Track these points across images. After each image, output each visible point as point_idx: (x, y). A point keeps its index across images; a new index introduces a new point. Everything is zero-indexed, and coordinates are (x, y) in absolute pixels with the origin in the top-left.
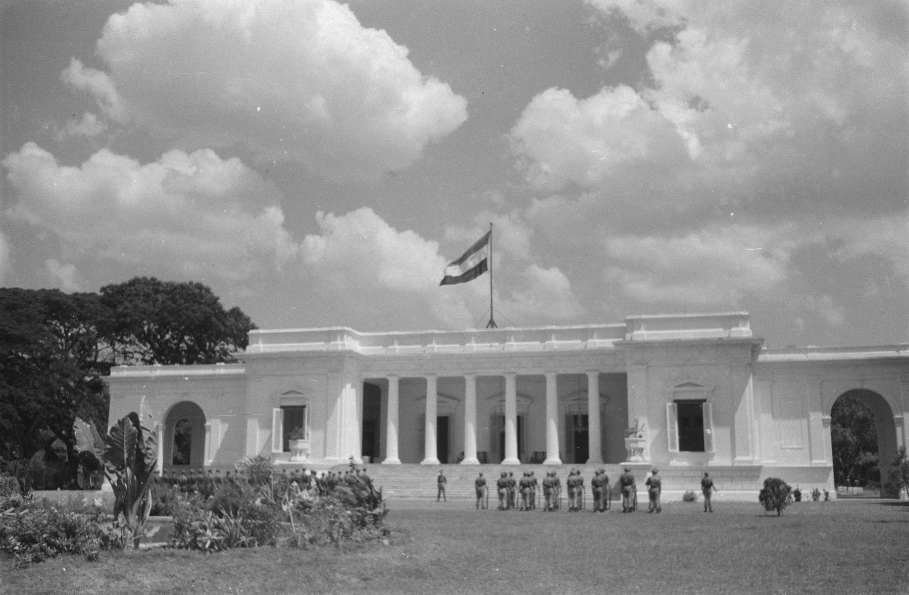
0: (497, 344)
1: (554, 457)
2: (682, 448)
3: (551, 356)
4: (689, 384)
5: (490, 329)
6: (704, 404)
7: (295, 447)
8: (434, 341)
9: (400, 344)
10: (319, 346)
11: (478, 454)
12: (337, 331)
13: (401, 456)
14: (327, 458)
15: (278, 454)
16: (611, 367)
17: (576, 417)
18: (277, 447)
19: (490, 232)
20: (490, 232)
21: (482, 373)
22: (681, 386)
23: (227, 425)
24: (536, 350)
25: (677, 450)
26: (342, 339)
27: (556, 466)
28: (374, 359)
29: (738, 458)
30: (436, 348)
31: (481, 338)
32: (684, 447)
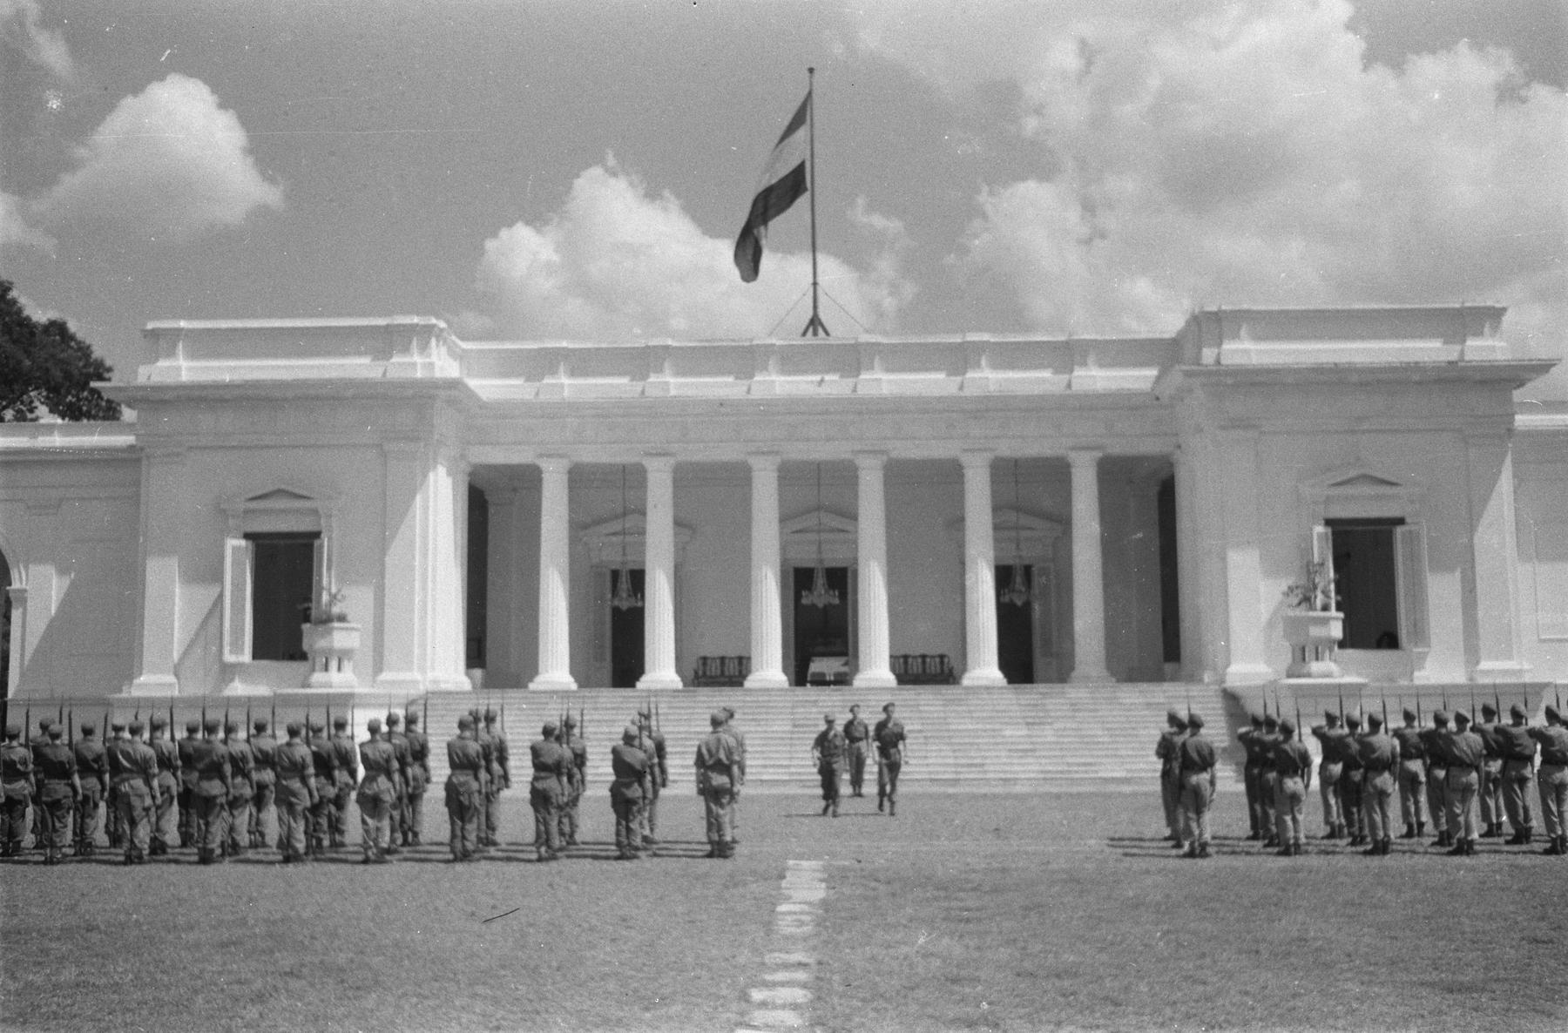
1: (556, 668)
2: (257, 655)
3: (770, 410)
5: (810, 339)
7: (321, 644)
8: (1091, 359)
10: (358, 367)
12: (413, 327)
13: (1004, 665)
14: (385, 676)
15: (241, 665)
17: (615, 575)
19: (810, 94)
20: (810, 94)
21: (799, 452)
24: (936, 393)
25: (246, 657)
26: (424, 348)
27: (565, 694)
28: (502, 412)
29: (1485, 665)
30: (671, 384)
31: (791, 360)
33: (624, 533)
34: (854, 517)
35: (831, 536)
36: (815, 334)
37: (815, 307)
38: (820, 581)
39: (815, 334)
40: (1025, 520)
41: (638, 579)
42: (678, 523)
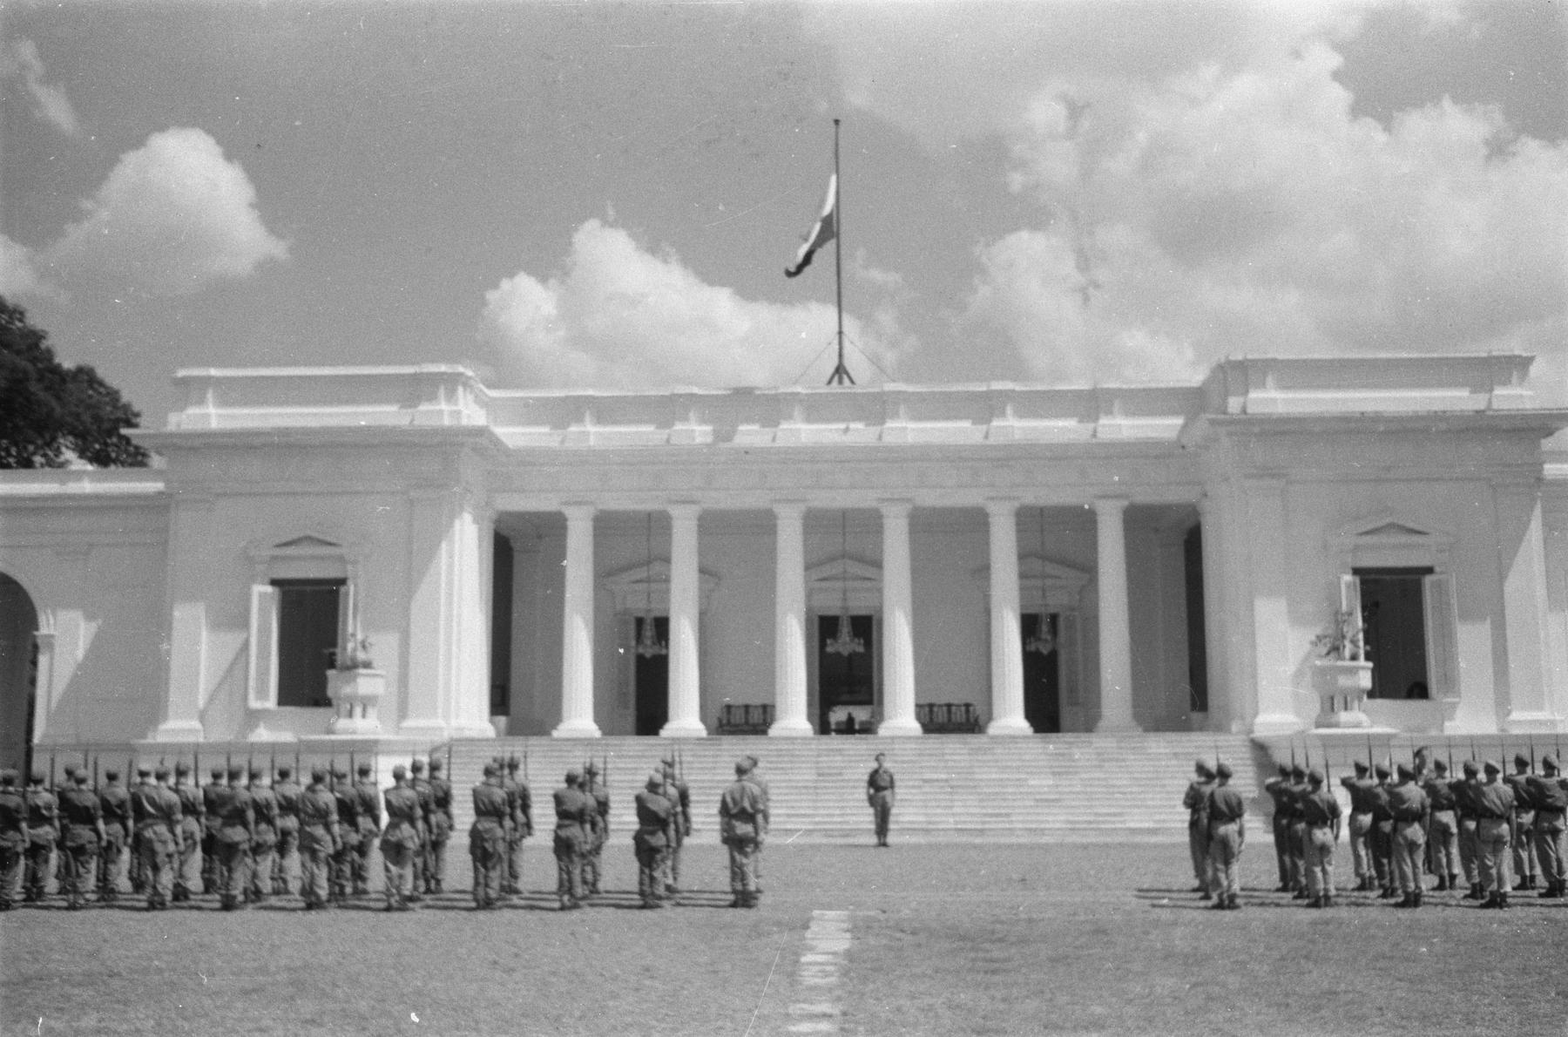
0: (860, 426)
1: (579, 716)
3: (582, 460)
4: (1391, 526)
6: (1428, 580)
7: (347, 690)
9: (600, 419)
11: (918, 706)
13: (1031, 714)
14: (407, 724)
16: (1165, 491)
17: (640, 622)
18: (262, 693)
22: (1367, 533)
23: (94, 626)
26: (451, 396)
32: (1381, 689)
33: (648, 580)
34: (878, 564)
35: (857, 584)
36: (840, 382)
37: (840, 355)
38: (845, 630)
39: (840, 382)
40: (1050, 569)
41: (662, 627)
42: (703, 571)
